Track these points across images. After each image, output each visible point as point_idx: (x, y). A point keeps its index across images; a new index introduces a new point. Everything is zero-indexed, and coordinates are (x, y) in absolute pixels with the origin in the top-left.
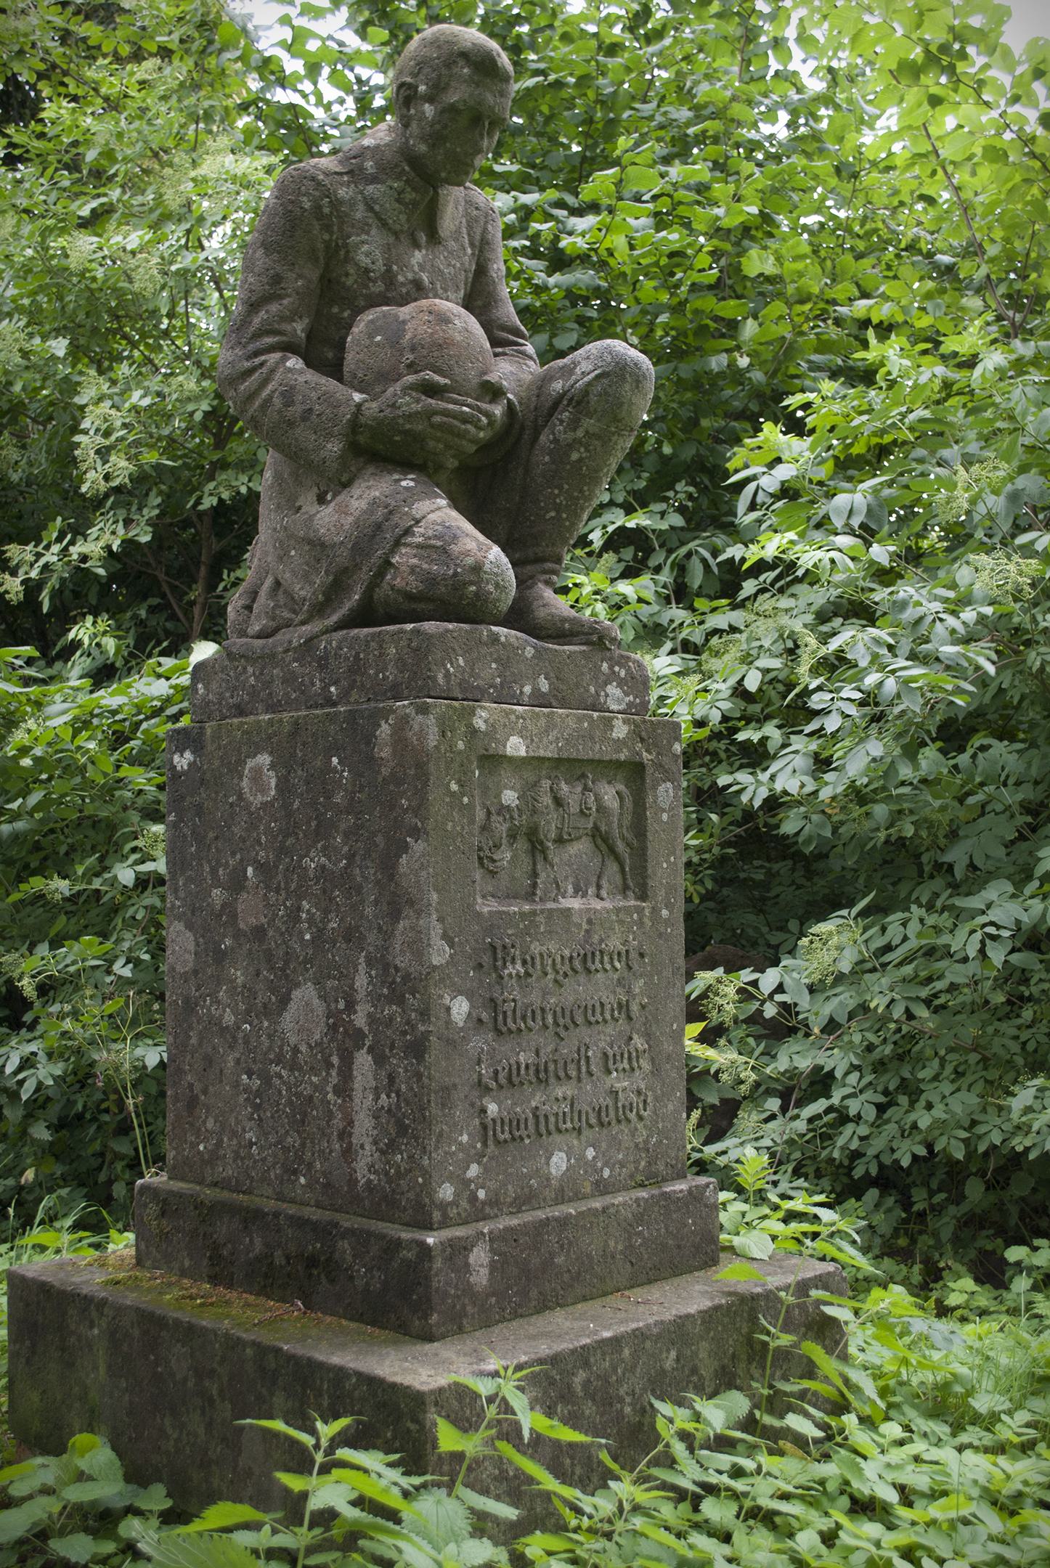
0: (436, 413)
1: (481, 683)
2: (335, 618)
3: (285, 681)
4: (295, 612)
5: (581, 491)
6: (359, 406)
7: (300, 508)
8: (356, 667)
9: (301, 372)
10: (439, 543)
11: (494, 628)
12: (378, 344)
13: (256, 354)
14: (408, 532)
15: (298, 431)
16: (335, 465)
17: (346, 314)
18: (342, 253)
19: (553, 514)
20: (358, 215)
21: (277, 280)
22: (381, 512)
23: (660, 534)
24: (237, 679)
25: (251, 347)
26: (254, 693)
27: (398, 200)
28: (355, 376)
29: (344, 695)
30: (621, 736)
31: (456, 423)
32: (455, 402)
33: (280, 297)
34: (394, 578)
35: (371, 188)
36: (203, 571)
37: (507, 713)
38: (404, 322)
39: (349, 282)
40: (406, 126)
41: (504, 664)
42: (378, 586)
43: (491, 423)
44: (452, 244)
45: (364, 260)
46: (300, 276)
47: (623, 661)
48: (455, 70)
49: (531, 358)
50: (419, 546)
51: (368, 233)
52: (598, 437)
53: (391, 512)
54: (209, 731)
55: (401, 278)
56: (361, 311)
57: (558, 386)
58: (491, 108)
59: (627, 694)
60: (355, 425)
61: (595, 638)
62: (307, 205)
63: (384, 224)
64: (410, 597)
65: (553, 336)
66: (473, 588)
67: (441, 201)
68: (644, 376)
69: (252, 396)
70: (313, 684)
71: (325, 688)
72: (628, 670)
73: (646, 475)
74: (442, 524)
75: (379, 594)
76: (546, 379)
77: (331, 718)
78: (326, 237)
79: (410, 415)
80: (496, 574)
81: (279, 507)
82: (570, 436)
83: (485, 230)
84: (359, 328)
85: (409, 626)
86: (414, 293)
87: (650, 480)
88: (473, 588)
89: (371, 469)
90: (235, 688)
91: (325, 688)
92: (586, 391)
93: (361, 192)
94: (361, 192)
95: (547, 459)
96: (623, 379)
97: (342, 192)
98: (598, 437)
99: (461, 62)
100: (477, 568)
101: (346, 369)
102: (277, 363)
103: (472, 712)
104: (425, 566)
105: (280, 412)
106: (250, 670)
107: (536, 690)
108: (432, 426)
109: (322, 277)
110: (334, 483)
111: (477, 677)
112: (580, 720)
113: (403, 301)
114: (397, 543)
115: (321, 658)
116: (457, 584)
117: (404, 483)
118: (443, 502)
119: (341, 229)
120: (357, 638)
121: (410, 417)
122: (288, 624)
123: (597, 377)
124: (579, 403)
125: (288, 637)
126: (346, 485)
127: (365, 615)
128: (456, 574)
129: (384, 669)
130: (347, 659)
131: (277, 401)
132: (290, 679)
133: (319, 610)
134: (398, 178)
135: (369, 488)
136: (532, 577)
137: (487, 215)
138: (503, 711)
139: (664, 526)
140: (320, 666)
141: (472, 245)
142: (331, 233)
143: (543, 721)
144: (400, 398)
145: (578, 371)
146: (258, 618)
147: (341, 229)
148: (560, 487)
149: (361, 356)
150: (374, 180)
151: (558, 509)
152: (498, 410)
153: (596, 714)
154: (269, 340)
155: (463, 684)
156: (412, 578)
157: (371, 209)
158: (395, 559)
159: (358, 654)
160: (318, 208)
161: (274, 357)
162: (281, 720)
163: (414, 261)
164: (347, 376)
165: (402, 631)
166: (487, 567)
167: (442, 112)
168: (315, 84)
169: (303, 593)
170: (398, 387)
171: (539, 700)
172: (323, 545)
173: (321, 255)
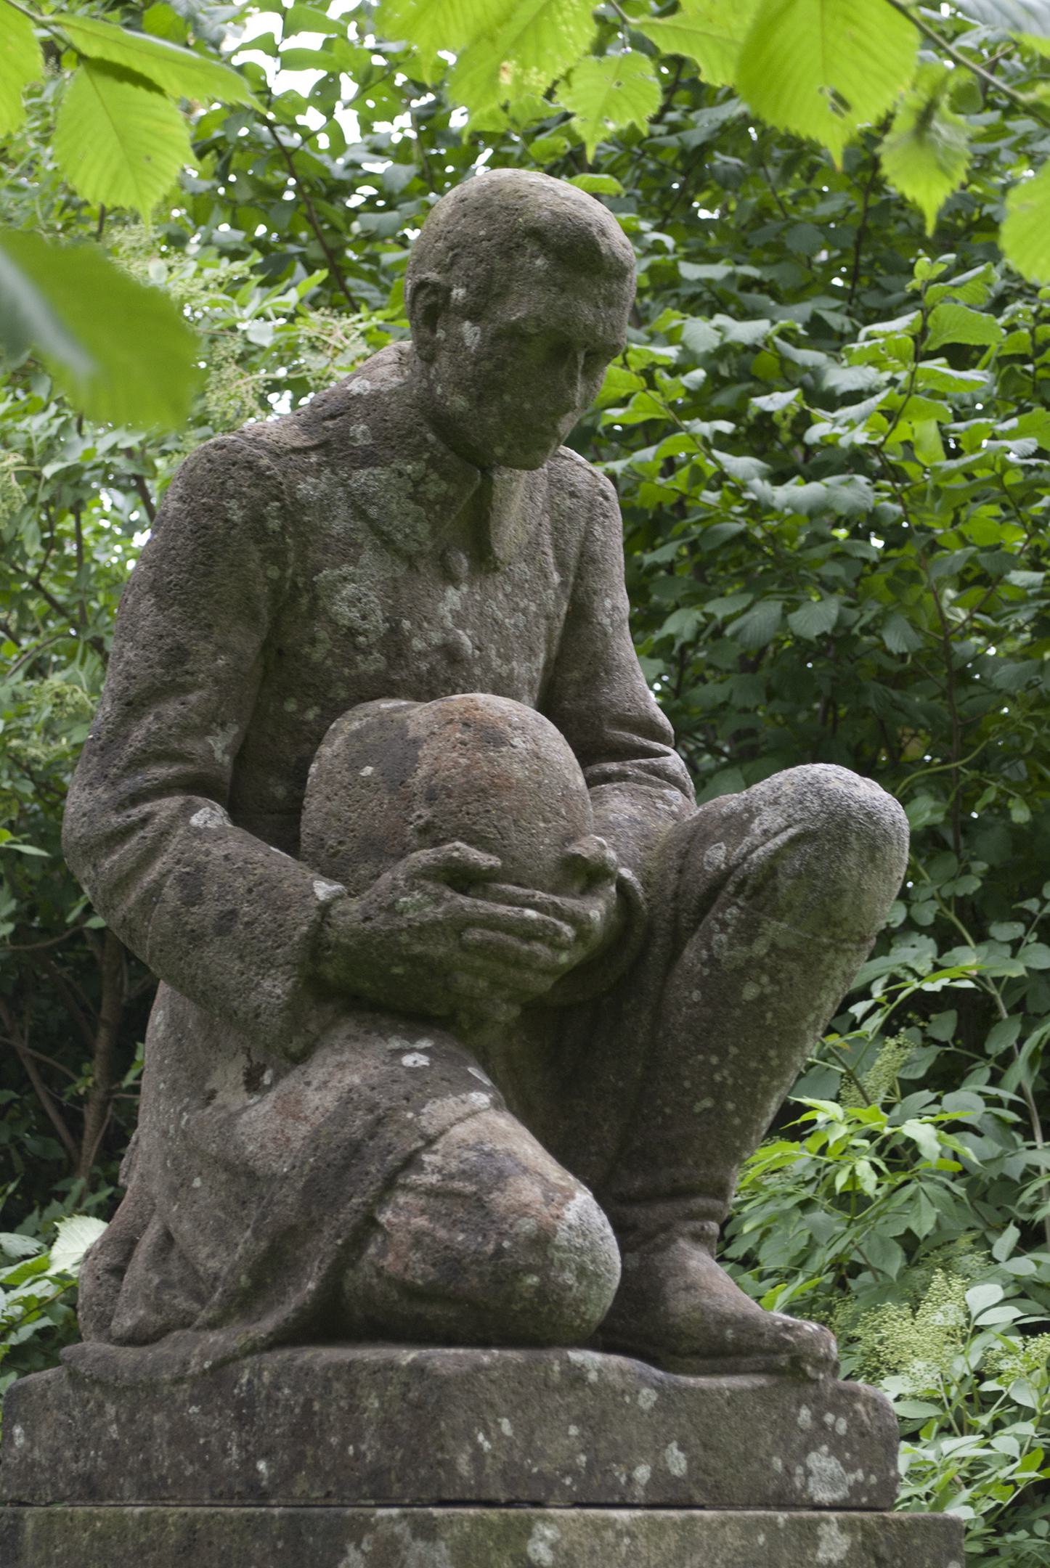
0: (471, 922)
1: (547, 1466)
2: (268, 1324)
3: (174, 1440)
4: (200, 1298)
5: (764, 1059)
6: (325, 908)
7: (212, 1095)
8: (306, 1429)
9: (218, 836)
10: (470, 1188)
11: (577, 1356)
12: (366, 783)
13: (136, 798)
14: (411, 1162)
15: (209, 953)
16: (278, 1022)
17: (311, 715)
18: (304, 601)
19: (708, 1103)
20: (337, 527)
21: (178, 656)
22: (360, 1120)
23: (1011, 985)
24: (86, 1423)
25: (127, 785)
26: (115, 1455)
27: (412, 497)
28: (321, 843)
29: (284, 1477)
30: (835, 1556)
31: (511, 940)
32: (511, 901)
33: (184, 689)
34: (382, 1254)
35: (362, 475)
36: (103, 1039)
37: (599, 1528)
38: (416, 743)
39: (318, 654)
40: (429, 360)
41: (594, 1424)
42: (353, 1265)
43: (582, 936)
44: (522, 569)
45: (346, 613)
46: (222, 649)
47: (844, 1401)
48: (520, 261)
49: (674, 781)
50: (432, 1192)
51: (354, 562)
52: (795, 955)
53: (379, 1121)
54: (30, 1526)
55: (418, 644)
56: (336, 710)
57: (717, 855)
58: (590, 330)
59: (849, 1468)
60: (316, 945)
61: (783, 1360)
62: (237, 516)
63: (386, 542)
64: (411, 1292)
65: (791, 606)
66: (533, 1280)
67: (498, 492)
68: (886, 837)
69: (124, 881)
70: (225, 1452)
71: (249, 1462)
72: (854, 1421)
73: (981, 866)
74: (477, 1147)
75: (355, 1280)
76: (697, 837)
77: (255, 1526)
78: (274, 573)
79: (422, 928)
80: (581, 1251)
81: (174, 1087)
82: (741, 952)
83: (588, 536)
84: (331, 750)
85: (407, 1356)
86: (444, 671)
87: (988, 877)
88: (533, 1280)
89: (348, 1027)
90: (81, 1443)
91: (249, 1462)
92: (771, 868)
93: (344, 483)
94: (344, 483)
95: (696, 995)
96: (844, 844)
97: (306, 487)
98: (795, 955)
99: (531, 247)
100: (542, 1240)
101: (305, 829)
102: (174, 819)
103: (526, 1530)
104: (442, 1233)
105: (175, 914)
106: (111, 1410)
107: (660, 1474)
108: (464, 948)
109: (266, 646)
110: (279, 1053)
111: (540, 1455)
112: (749, 1529)
113: (426, 690)
114: (390, 1184)
115: (240, 1403)
116: (503, 1272)
117: (408, 1060)
118: (480, 1099)
119: (302, 557)
120: (307, 1371)
121: (423, 931)
122: (186, 1322)
123: (794, 841)
124: (757, 891)
125: (181, 1352)
126: (301, 1058)
127: (329, 1321)
128: (499, 1251)
129: (357, 1438)
130: (289, 1409)
131: (171, 894)
132: (183, 1436)
133: (243, 1303)
134: (414, 456)
135: (341, 1066)
136: (666, 1228)
137: (592, 505)
138: (589, 1522)
139: (1016, 970)
140: (239, 1417)
141: (561, 565)
142: (283, 566)
143: (671, 1539)
144: (404, 895)
145: (756, 827)
146: (131, 1302)
147: (302, 557)
148: (722, 1053)
149: (333, 805)
150: (368, 458)
151: (718, 1093)
152: (596, 910)
153: (782, 1517)
154: (160, 772)
155: (511, 1473)
156: (415, 1256)
157: (361, 514)
158: (386, 1217)
159: (308, 1403)
160: (257, 520)
161: (168, 805)
162: (163, 1520)
163: (444, 609)
164: (306, 842)
165: (391, 1366)
166: (562, 1237)
167: (497, 337)
168: (329, 113)
169: (213, 1264)
170: (396, 874)
171: (668, 1495)
172: (252, 1175)
173: (264, 609)
